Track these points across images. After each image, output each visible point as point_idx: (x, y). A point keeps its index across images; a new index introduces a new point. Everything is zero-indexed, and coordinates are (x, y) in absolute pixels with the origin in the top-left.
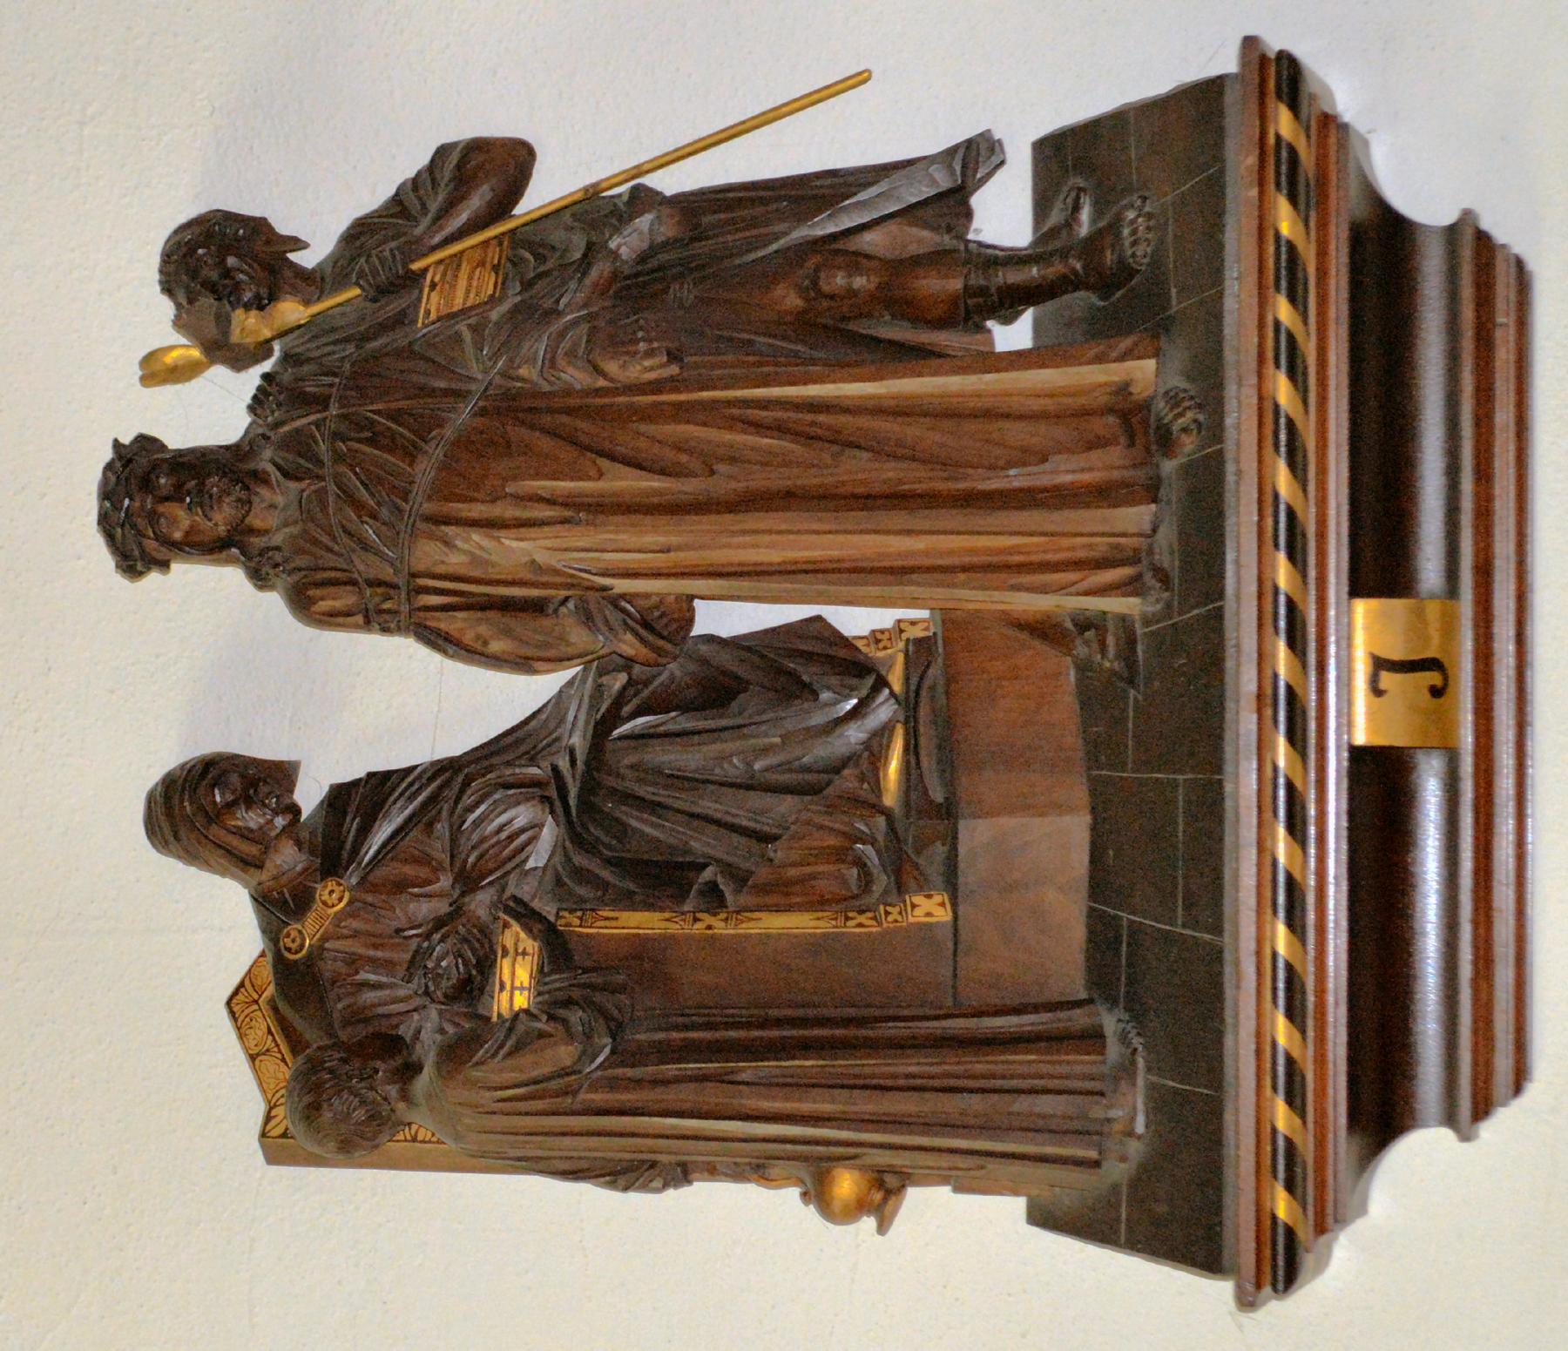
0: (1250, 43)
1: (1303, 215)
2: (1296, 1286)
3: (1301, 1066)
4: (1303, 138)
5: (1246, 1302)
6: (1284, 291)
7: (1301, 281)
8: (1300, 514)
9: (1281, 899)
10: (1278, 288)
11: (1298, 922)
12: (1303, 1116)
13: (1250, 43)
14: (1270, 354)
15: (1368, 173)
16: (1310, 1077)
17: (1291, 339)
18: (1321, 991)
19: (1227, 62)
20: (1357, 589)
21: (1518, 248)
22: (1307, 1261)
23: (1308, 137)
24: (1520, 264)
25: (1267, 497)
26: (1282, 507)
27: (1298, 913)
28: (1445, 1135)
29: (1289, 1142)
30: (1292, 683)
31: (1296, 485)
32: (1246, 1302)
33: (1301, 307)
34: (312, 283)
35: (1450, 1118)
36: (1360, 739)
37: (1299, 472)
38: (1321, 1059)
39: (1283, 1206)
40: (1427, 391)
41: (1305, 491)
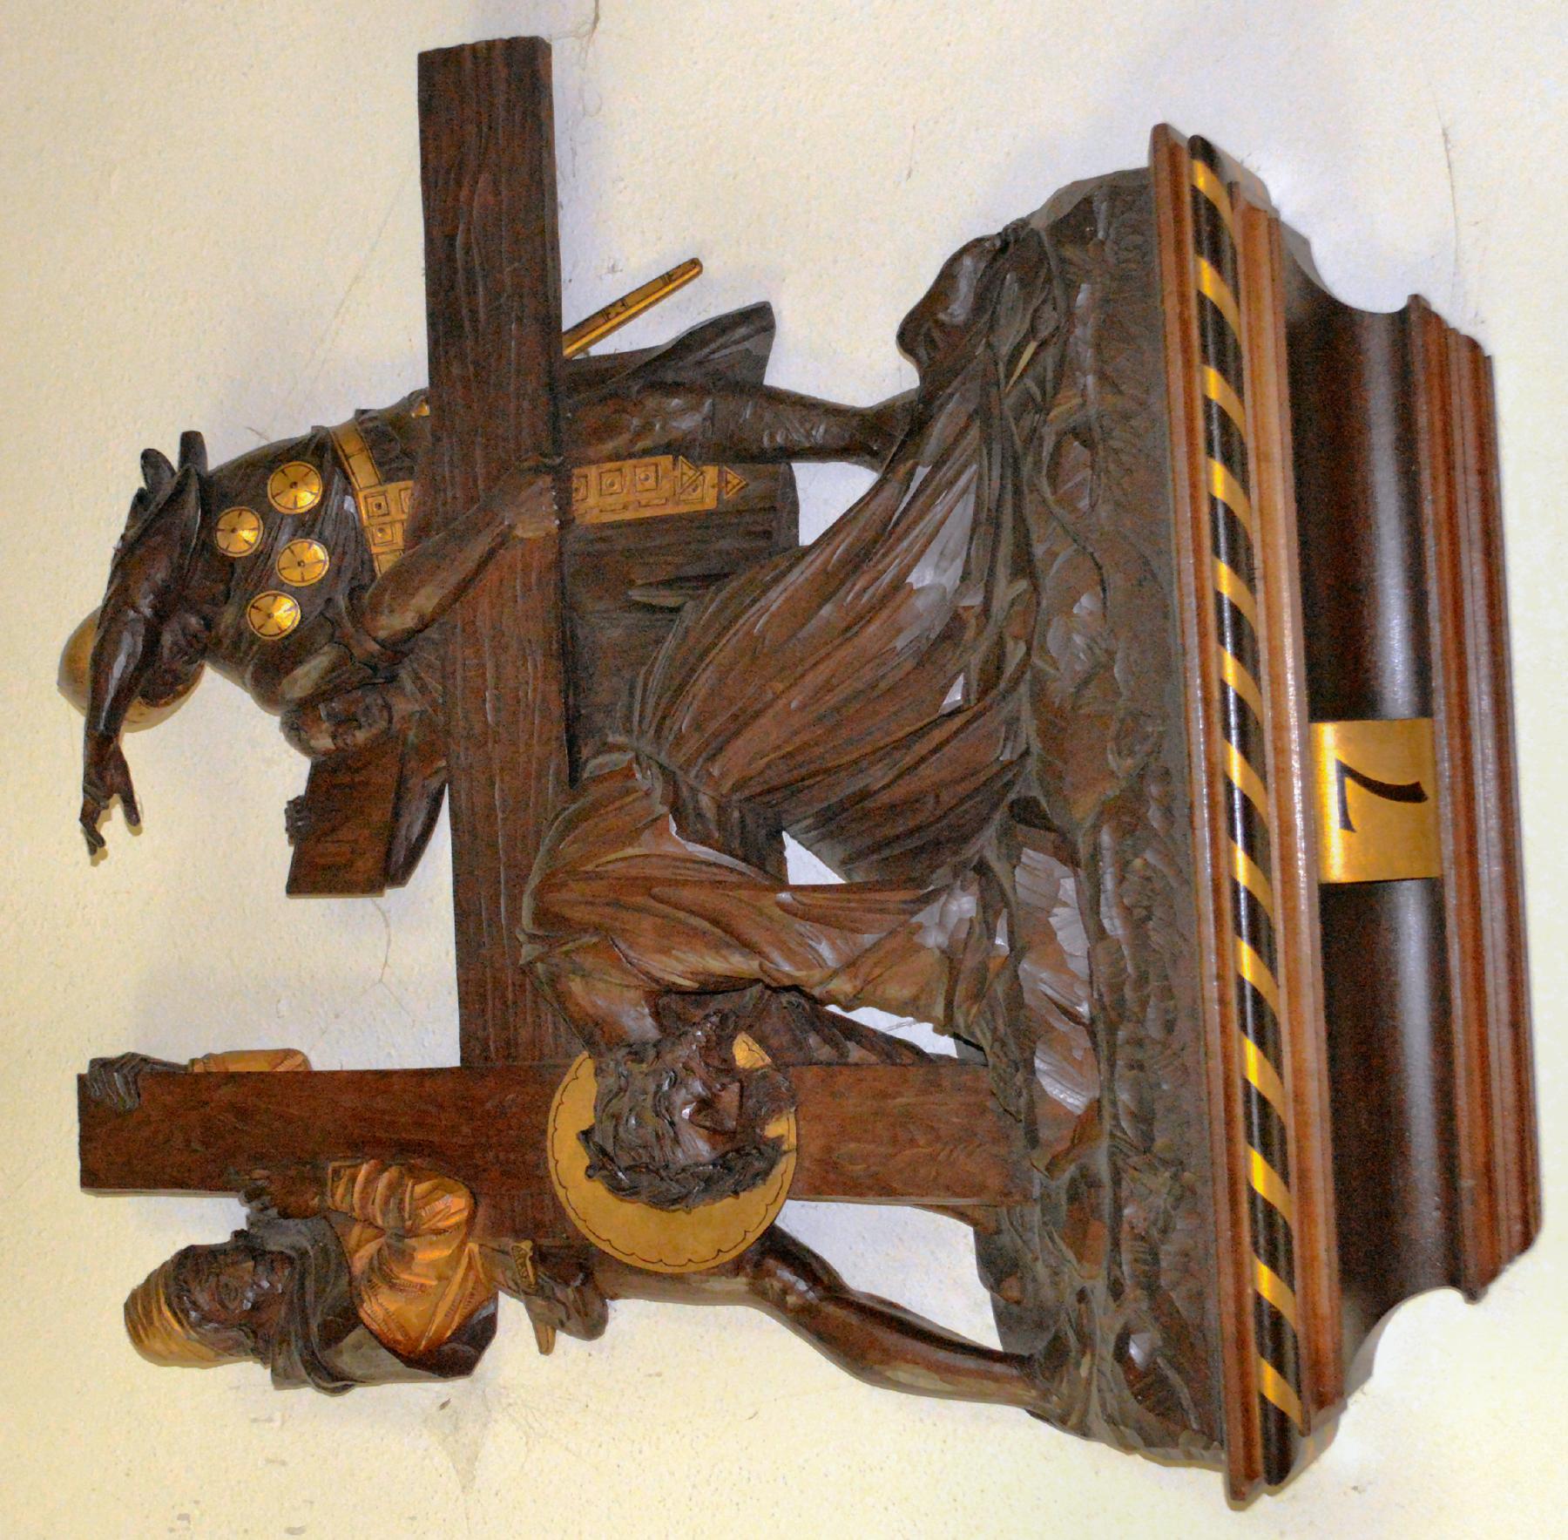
0: (1162, 134)
1: (1239, 476)
2: (1291, 1475)
3: (1268, 910)
4: (1293, 1397)
5: (1238, 1495)
6: (1224, 558)
7: (1232, 347)
8: (1270, 1001)
9: (1233, 720)
10: (1205, 360)
11: (1252, 747)
12: (1272, 967)
13: (1162, 134)
14: (1207, 543)
15: (1312, 276)
16: (1279, 926)
17: (1258, 998)
18: (1302, 1125)
19: (1136, 156)
20: (1322, 706)
21: (1466, 329)
22: (1304, 1445)
23: (1299, 1392)
24: (1474, 346)
25: (1222, 881)
26: (1226, 607)
27: (1253, 739)
28: (1449, 1298)
29: (1250, 897)
30: (1240, 693)
31: (1245, 673)
32: (1238, 1495)
33: (1238, 469)
34: (533, 1241)
35: (1454, 1279)
36: (1338, 870)
37: (1271, 1050)
38: (1298, 1097)
39: (1270, 1382)
40: (1429, 1095)
41: (1280, 1075)
